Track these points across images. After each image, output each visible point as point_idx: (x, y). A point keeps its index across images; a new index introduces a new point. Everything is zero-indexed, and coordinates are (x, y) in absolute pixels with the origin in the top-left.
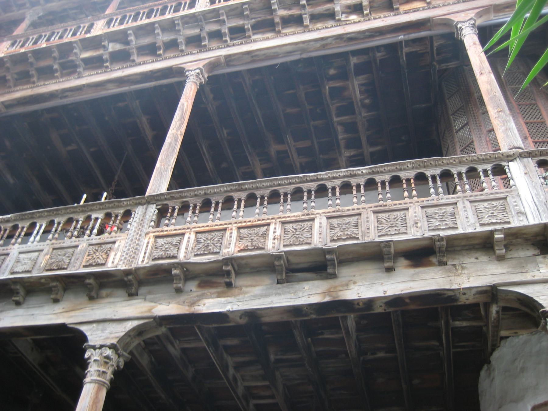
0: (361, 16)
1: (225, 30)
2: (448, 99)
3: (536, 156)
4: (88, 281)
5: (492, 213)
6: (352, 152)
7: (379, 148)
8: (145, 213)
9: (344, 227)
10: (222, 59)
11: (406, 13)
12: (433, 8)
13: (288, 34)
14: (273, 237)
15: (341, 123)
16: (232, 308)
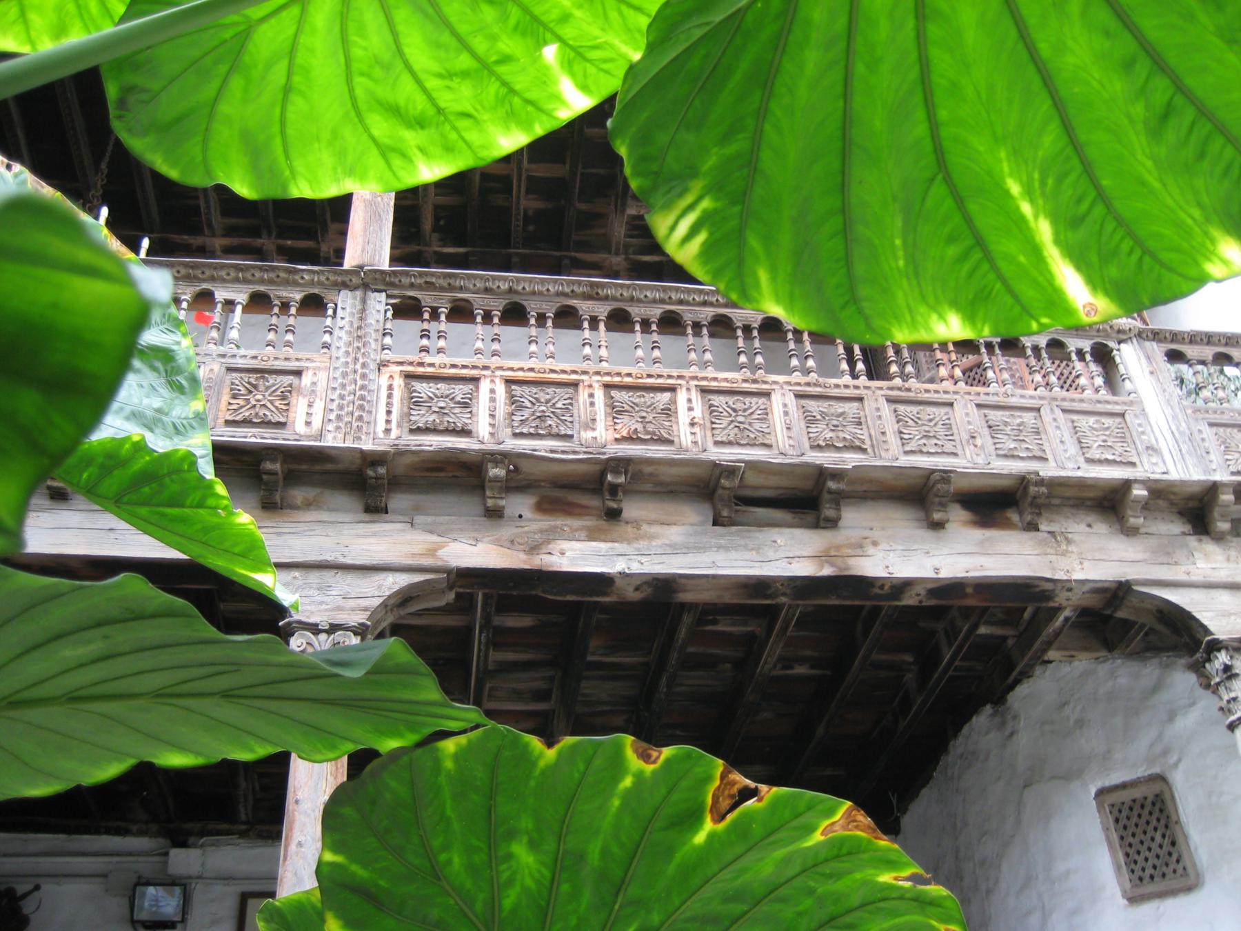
5: (1105, 441)
8: (363, 310)
14: (688, 421)
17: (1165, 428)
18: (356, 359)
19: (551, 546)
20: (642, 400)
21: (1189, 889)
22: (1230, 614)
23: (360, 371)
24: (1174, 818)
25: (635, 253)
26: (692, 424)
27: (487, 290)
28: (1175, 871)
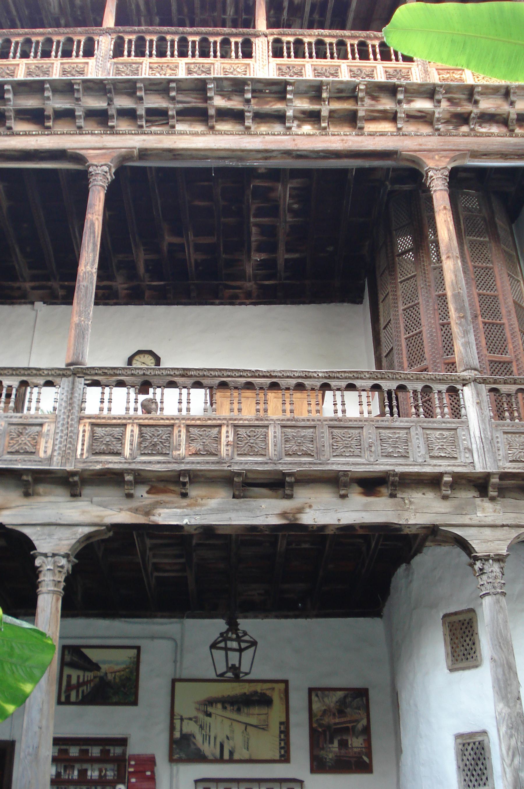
0: (316, 126)
1: (141, 111)
2: (396, 230)
3: (489, 383)
4: (25, 478)
5: (442, 445)
6: (263, 256)
7: (296, 256)
8: (73, 388)
9: (299, 441)
10: (135, 153)
11: (370, 135)
12: (403, 135)
13: (223, 133)
14: (225, 443)
15: (256, 225)
16: (190, 522)
17: (477, 434)
18: (69, 416)
19: (155, 511)
20: (204, 432)
21: (476, 667)
22: (489, 541)
23: (70, 423)
24: (475, 631)
25: (260, 280)
26: (227, 445)
27: (132, 375)
28: (472, 657)
